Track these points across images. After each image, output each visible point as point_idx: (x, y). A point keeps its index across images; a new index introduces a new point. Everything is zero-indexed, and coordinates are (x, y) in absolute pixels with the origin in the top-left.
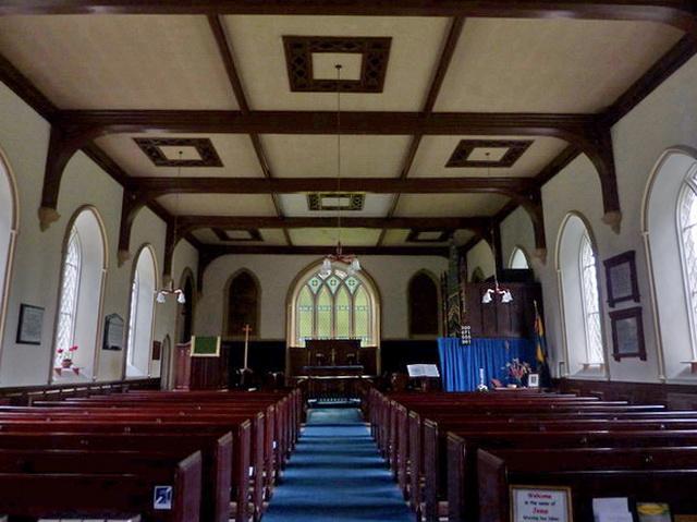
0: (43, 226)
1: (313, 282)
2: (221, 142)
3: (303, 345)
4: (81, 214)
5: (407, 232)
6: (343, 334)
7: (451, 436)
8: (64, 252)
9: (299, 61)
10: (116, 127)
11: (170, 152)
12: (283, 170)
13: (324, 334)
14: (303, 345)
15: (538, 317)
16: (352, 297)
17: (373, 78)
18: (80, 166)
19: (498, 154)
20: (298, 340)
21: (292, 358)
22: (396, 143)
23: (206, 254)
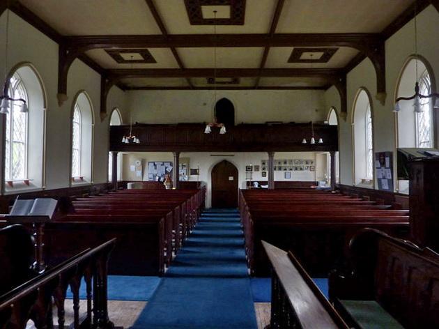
0: (60, 103)
2: (154, 52)
4: (79, 97)
5: (288, 51)
8: (72, 117)
9: (194, 10)
10: (96, 45)
11: (126, 56)
15: (55, 310)
17: (238, 17)
18: (77, 67)
19: (318, 55)
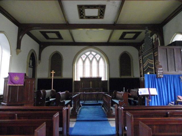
1: (84, 57)
3: (79, 80)
6: (95, 75)
7: (128, 113)
12: (78, 39)
13: (87, 75)
14: (79, 80)
16: (98, 62)
17: (101, 14)
20: (77, 78)
21: (75, 85)
22: (108, 32)
23: (42, 45)
